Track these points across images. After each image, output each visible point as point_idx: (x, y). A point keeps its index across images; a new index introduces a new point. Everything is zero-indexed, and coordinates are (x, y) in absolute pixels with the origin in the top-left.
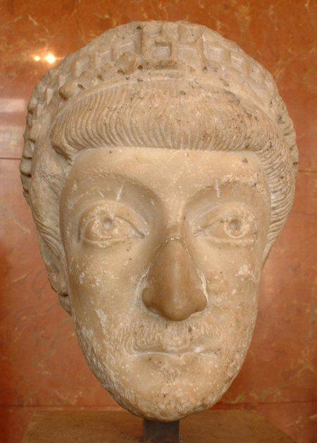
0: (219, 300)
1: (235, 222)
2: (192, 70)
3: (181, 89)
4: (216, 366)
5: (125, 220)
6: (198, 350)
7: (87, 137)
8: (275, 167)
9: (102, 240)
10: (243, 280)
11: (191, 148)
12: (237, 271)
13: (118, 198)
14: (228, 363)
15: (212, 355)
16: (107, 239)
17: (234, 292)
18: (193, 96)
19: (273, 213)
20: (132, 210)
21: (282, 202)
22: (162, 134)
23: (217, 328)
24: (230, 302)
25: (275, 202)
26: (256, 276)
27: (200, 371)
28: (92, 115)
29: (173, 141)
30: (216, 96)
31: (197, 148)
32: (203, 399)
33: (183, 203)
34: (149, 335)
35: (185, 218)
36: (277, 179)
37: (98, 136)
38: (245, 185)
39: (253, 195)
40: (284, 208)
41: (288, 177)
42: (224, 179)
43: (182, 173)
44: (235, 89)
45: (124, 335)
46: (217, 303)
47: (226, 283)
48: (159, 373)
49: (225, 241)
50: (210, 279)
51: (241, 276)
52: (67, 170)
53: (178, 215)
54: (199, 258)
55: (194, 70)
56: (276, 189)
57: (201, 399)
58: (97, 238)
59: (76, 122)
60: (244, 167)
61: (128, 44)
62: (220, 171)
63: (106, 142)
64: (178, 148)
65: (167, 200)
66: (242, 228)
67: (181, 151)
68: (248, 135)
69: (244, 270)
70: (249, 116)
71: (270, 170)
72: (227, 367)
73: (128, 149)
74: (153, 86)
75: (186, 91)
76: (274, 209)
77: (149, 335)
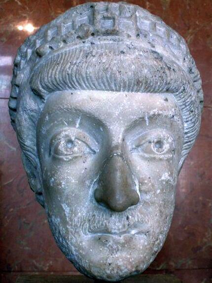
0: (148, 197)
1: (159, 143)
2: (129, 36)
3: (121, 49)
4: (146, 244)
5: (82, 141)
6: (133, 232)
7: (55, 83)
8: (187, 104)
9: (66, 155)
10: (164, 183)
11: (128, 91)
12: (161, 177)
13: (77, 126)
14: (154, 242)
15: (143, 236)
16: (70, 155)
17: (159, 191)
18: (130, 54)
19: (186, 136)
20: (87, 134)
21: (192, 128)
22: (108, 81)
23: (147, 217)
24: (155, 198)
25: (187, 129)
26: (174, 180)
27: (134, 247)
28: (59, 68)
29: (116, 86)
30: (146, 54)
31: (132, 91)
32: (137, 266)
33: (123, 129)
34: (99, 222)
35: (124, 140)
36: (188, 113)
37: (63, 82)
38: (166, 116)
39: (172, 124)
40: (194, 133)
41: (196, 111)
42: (152, 113)
43: (122, 108)
44: (159, 50)
45: (81, 222)
46: (147, 199)
47: (153, 185)
48: (106, 248)
49: (152, 156)
50: (141, 183)
51: (163, 180)
52: (42, 106)
53: (119, 138)
54: (134, 168)
55: (130, 36)
56: (188, 120)
57: (135, 266)
58: (62, 154)
59: (48, 73)
60: (165, 104)
61: (85, 18)
62: (148, 107)
63: (88, 88)
64: (119, 91)
65: (111, 128)
66: (164, 147)
67: (122, 93)
68: (168, 82)
69: (165, 176)
70: (169, 68)
71: (184, 106)
72: (153, 244)
73: (84, 91)
74: (102, 47)
75: (125, 50)
76: (186, 133)
77: (99, 222)
